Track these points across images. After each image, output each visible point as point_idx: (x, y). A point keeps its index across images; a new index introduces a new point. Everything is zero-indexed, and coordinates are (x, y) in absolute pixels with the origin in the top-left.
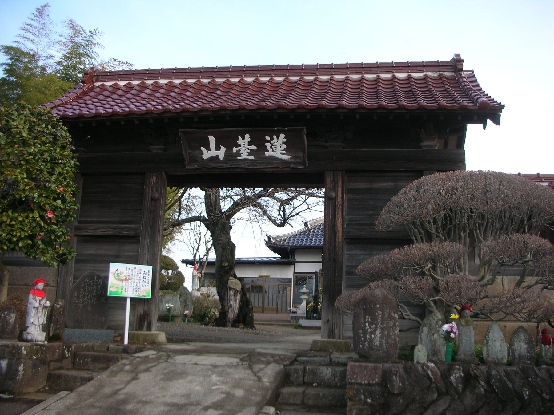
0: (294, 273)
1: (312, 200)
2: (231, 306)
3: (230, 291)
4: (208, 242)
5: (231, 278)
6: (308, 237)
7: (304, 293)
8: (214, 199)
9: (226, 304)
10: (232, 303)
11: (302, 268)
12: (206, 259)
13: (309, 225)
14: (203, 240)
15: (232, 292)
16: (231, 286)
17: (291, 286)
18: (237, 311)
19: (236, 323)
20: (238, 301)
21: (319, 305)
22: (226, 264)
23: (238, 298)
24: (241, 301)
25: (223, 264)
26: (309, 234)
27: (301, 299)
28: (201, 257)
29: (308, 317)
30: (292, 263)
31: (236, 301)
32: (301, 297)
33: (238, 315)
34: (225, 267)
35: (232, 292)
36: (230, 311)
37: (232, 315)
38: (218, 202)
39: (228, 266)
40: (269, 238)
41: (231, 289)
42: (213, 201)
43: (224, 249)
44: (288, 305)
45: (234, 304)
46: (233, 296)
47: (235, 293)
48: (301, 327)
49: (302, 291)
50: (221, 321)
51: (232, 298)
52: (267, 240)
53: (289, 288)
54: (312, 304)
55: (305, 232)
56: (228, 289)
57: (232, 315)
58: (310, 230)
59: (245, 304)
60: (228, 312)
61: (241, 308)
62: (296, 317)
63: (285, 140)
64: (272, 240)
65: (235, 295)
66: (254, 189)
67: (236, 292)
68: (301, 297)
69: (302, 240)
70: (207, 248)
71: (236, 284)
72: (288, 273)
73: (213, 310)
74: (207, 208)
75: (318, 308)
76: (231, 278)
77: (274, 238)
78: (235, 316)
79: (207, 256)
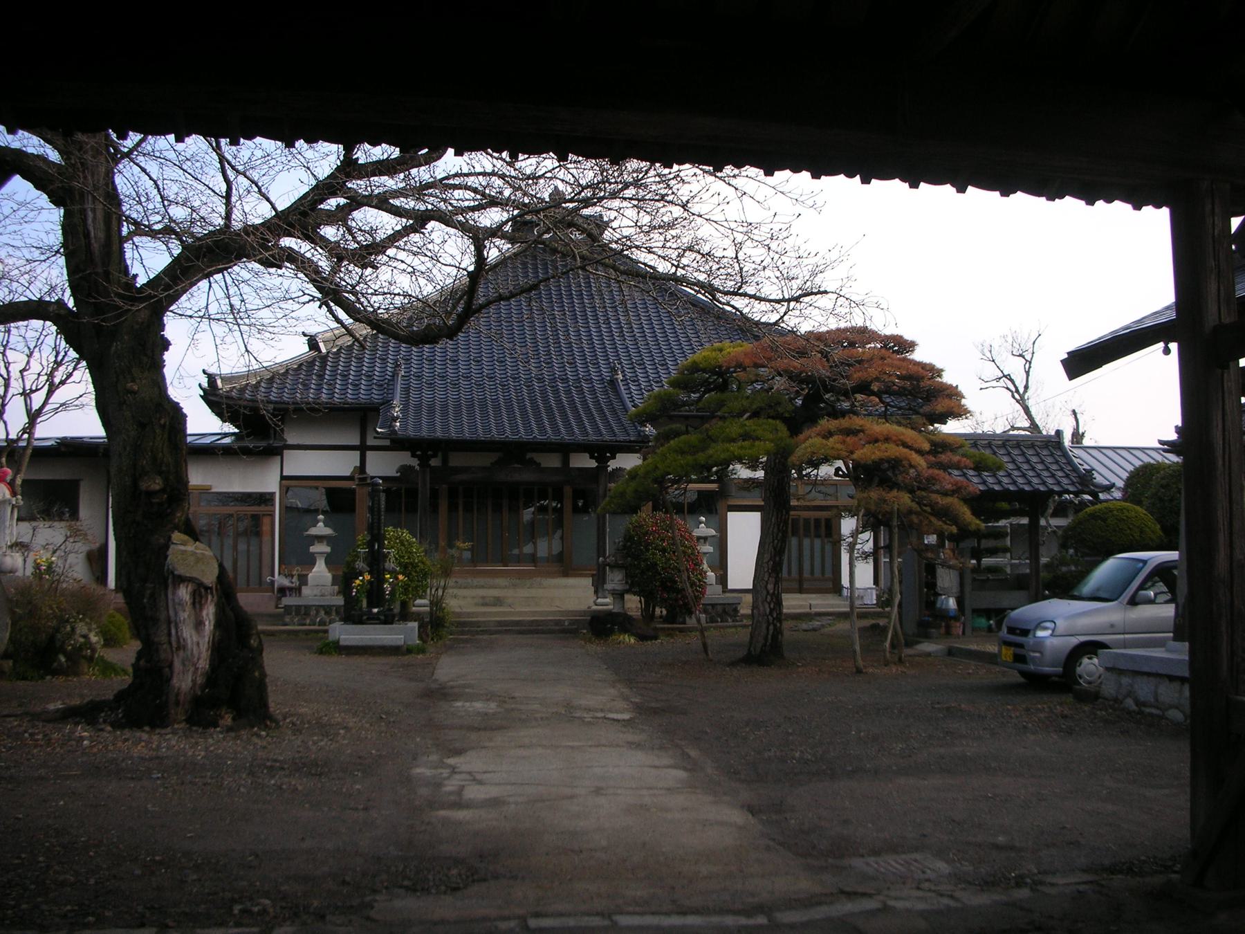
0: (283, 478)
1: (721, 245)
2: (181, 646)
3: (176, 586)
4: (32, 391)
5: (177, 536)
6: (321, 377)
7: (320, 538)
8: (101, 235)
9: (164, 639)
10: (188, 633)
11: (304, 464)
12: (29, 440)
13: (322, 345)
14: (16, 387)
15: (184, 593)
16: (181, 570)
17: (272, 516)
18: (204, 664)
19: (201, 712)
20: (209, 626)
21: (387, 581)
22: (156, 484)
23: (209, 612)
24: (219, 624)
25: (143, 485)
26: (323, 367)
27: (313, 554)
28: (13, 436)
29: (351, 615)
30: (274, 451)
31: (199, 624)
32: (312, 549)
33: (212, 678)
34: (150, 494)
35: (184, 593)
36: (177, 665)
37: (184, 681)
38: (115, 247)
39: (163, 491)
40: (211, 378)
41: (182, 579)
42: (96, 246)
43: (142, 426)
44: (266, 570)
45: (195, 635)
46: (188, 608)
47: (194, 594)
48: (338, 649)
49: (313, 531)
50: (144, 702)
51: (185, 615)
52: (205, 385)
53: (266, 521)
54: (367, 577)
55: (311, 363)
56: (168, 579)
57: (184, 681)
58: (324, 359)
59: (235, 634)
60: (171, 666)
61: (219, 649)
62: (298, 607)
63: (171, 137)
64: (219, 382)
65: (198, 599)
66: (514, 157)
67: (200, 592)
68: (312, 549)
69: (306, 387)
70: (29, 411)
71: (199, 559)
72: (266, 480)
73: (81, 628)
74: (72, 270)
75: (383, 590)
76: (177, 536)
77: (225, 379)
78: (199, 680)
79: (31, 434)
